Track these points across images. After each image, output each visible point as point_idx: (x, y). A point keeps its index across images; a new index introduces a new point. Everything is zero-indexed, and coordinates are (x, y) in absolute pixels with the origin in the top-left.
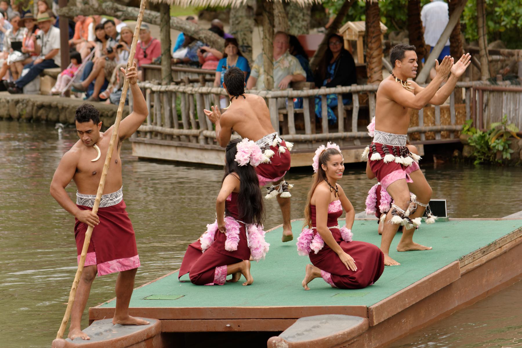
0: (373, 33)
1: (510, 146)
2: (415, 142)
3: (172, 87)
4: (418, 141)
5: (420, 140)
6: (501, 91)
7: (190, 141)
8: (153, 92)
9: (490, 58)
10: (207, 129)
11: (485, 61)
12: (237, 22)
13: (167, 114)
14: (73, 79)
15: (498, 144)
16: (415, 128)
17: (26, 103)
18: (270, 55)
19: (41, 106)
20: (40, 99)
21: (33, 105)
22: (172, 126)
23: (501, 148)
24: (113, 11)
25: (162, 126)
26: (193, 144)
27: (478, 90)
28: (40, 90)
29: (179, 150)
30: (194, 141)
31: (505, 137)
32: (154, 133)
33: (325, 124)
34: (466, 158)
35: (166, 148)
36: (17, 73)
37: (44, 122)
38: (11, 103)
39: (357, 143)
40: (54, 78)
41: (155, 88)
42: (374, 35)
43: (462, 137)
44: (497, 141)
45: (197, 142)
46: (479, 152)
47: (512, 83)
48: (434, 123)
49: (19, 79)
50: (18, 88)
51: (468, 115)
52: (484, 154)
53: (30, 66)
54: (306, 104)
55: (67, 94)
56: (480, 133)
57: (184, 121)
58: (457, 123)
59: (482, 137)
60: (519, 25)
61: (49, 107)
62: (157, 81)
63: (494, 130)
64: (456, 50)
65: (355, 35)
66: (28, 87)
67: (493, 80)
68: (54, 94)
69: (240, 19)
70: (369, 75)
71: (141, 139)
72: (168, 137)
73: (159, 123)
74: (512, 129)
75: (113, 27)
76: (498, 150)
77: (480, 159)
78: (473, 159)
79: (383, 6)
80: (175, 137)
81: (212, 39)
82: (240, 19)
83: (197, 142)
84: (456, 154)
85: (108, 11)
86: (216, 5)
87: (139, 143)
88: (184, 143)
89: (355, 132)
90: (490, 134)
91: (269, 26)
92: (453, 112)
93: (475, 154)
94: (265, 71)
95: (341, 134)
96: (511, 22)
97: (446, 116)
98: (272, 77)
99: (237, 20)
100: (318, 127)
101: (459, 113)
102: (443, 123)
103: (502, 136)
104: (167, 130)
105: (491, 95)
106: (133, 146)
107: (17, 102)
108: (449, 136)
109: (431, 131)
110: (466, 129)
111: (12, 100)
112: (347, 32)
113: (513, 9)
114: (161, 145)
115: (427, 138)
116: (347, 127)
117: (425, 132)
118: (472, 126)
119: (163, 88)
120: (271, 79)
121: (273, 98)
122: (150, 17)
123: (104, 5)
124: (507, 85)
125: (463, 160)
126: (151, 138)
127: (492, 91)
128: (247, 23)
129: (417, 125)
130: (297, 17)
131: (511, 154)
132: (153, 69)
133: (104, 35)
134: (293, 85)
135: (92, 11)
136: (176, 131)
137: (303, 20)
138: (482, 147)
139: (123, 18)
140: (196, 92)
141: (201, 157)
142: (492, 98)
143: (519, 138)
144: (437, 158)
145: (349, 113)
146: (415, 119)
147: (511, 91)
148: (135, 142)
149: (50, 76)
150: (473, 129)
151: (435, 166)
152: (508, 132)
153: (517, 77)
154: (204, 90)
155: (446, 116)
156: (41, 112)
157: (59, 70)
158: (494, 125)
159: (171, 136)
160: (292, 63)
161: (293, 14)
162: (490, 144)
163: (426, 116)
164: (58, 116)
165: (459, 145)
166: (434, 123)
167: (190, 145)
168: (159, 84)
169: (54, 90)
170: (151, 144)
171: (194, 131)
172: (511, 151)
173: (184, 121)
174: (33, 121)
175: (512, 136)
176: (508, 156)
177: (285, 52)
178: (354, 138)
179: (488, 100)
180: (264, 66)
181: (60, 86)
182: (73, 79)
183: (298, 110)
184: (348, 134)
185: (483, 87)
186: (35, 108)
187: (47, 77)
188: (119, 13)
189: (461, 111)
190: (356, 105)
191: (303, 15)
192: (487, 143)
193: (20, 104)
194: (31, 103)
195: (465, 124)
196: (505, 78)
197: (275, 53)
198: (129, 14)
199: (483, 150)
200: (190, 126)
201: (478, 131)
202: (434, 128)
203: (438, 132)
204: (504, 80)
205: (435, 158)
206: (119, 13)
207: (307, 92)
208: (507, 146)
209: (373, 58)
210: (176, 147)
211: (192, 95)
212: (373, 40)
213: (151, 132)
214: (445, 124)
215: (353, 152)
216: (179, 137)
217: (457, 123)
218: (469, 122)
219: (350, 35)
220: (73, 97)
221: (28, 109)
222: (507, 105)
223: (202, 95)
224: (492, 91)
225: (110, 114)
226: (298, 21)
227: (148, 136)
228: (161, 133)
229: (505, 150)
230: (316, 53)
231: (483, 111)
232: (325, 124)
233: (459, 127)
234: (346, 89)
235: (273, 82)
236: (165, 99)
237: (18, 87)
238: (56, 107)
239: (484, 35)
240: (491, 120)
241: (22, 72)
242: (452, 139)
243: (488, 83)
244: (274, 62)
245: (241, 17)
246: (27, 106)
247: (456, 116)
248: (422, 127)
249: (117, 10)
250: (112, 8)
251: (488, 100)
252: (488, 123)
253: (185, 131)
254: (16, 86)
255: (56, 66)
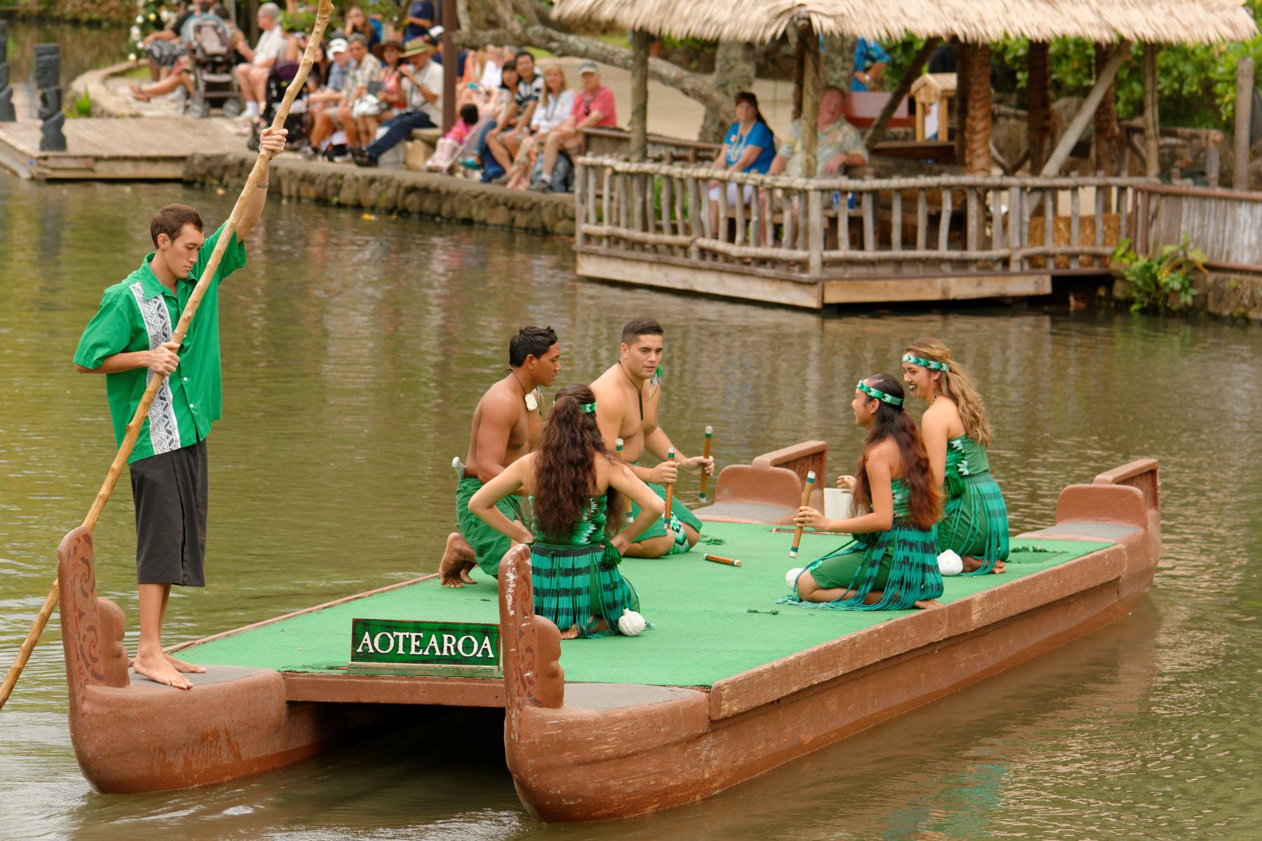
0: (978, 93)
1: (1192, 284)
2: (1037, 271)
3: (648, 167)
4: (1042, 270)
5: (1045, 267)
6: (1179, 196)
7: (673, 254)
8: (615, 173)
9: (1162, 142)
10: (703, 236)
11: (1153, 145)
12: (727, 67)
13: (637, 209)
14: (461, 148)
15: (1173, 279)
16: (1038, 249)
17: (387, 182)
18: (813, 121)
19: (412, 189)
20: (409, 178)
21: (399, 186)
22: (645, 228)
23: (1177, 286)
24: (544, 41)
25: (627, 227)
26: (680, 258)
27: (1142, 192)
28: (405, 163)
29: (655, 268)
30: (681, 254)
31: (1185, 269)
32: (615, 240)
33: (896, 235)
34: (1118, 301)
35: (635, 264)
36: (368, 133)
37: (415, 216)
38: (361, 181)
39: (946, 268)
40: (431, 145)
41: (621, 166)
42: (980, 96)
43: (1114, 266)
44: (1172, 275)
45: (686, 255)
46: (1139, 291)
47: (1196, 184)
48: (1069, 242)
49: (372, 142)
50: (370, 157)
51: (1124, 230)
52: (1148, 294)
53: (388, 123)
54: (867, 203)
55: (451, 171)
56: (1143, 261)
57: (665, 221)
58: (1104, 244)
59: (1147, 268)
60: (1185, 92)
61: (425, 191)
62: (623, 156)
63: (1167, 257)
64: (1105, 126)
65: (936, 95)
66: (386, 157)
67: (1165, 174)
68: (431, 170)
69: (733, 62)
70: (967, 160)
71: (593, 247)
72: (637, 247)
73: (623, 220)
74: (1197, 256)
75: (530, 65)
76: (1172, 290)
77: (1142, 302)
78: (1130, 301)
79: (265, 16)
80: (648, 246)
81: (703, 92)
82: (733, 62)
83: (686, 255)
84: (1102, 292)
85: (536, 41)
86: (732, 37)
87: (589, 254)
88: (666, 257)
89: (943, 251)
90: (1160, 263)
91: (814, 74)
92: (1100, 225)
93: (1135, 294)
94: (804, 147)
95: (921, 252)
96: (1171, 86)
97: (1088, 232)
98: (815, 157)
99: (728, 63)
100: (884, 240)
101: (1109, 227)
102: (1083, 243)
103: (1179, 267)
104: (637, 234)
105: (1163, 202)
106: (579, 258)
107: (372, 181)
108: (1091, 264)
109: (1063, 254)
110: (1120, 253)
111: (364, 177)
112: (922, 91)
113: (1175, 66)
114: (625, 259)
115: (1057, 266)
116: (932, 243)
117: (1053, 256)
118: (1129, 249)
119: (634, 167)
120: (813, 160)
121: (816, 190)
122: (605, 53)
123: (530, 31)
124: (1186, 185)
125: (1112, 304)
126: (609, 246)
127: (1164, 195)
128: (744, 70)
129: (1042, 243)
130: (832, 62)
131: (1194, 297)
132: (600, 137)
133: (514, 77)
134: (848, 169)
135: (509, 37)
136: (651, 237)
137: (843, 69)
138: (1146, 283)
139: (559, 52)
140: (688, 176)
141: (692, 281)
142: (1164, 205)
143: (1206, 272)
144: (1076, 299)
145: (934, 220)
146: (1038, 234)
147: (1196, 196)
148: (583, 253)
149: (423, 140)
150: (1132, 255)
151: (1072, 309)
152: (1189, 262)
153: (1203, 174)
154: (702, 172)
155: (1088, 232)
156: (412, 197)
157: (438, 131)
158: (1167, 250)
159: (642, 245)
160: (848, 138)
161: (827, 57)
162: (1159, 278)
163: (1057, 230)
164: (440, 206)
165: (1108, 280)
166: (1069, 242)
167: (674, 260)
168: (627, 160)
169: (430, 163)
170: (609, 257)
171: (681, 239)
172: (1194, 292)
173: (665, 221)
174: (398, 211)
175: (1196, 269)
176: (1189, 300)
177: (838, 119)
178: (941, 261)
179: (1157, 209)
180: (803, 139)
181: (441, 159)
182: (461, 148)
183: (854, 212)
184: (932, 254)
185: (1151, 187)
186: (402, 191)
187: (418, 143)
188: (554, 45)
189: (1112, 225)
190: (947, 208)
191: (844, 61)
192: (1154, 277)
193: (377, 184)
194: (394, 184)
195: (1119, 245)
196: (1185, 174)
197: (820, 121)
198: (569, 46)
199: (1148, 289)
200: (675, 230)
201: (1141, 257)
202: (1070, 249)
203: (1074, 256)
204: (1183, 177)
205: (1072, 299)
206: (554, 45)
207: (870, 183)
208: (1187, 284)
209: (977, 133)
210: (651, 263)
211: (681, 180)
212: (978, 105)
213: (608, 237)
214: (1086, 244)
215: (939, 282)
216: (655, 247)
217: (1104, 244)
218: (1125, 243)
219: (927, 95)
220: (459, 176)
221: (391, 193)
222: (1188, 218)
223: (697, 180)
224: (1164, 195)
225: (527, 205)
226: (834, 69)
227: (605, 243)
228: (625, 240)
229: (1184, 289)
230: (875, 123)
231: (1148, 225)
232: (896, 235)
233: (1108, 250)
234: (910, 182)
235: (816, 163)
236: (635, 185)
237: (370, 157)
238: (437, 191)
239: (1153, 105)
240: (1162, 240)
241: (375, 133)
242: (1095, 269)
243: (1158, 181)
244: (819, 134)
245: (735, 59)
246: (388, 187)
247: (1105, 233)
248: (1050, 247)
249: (551, 39)
250: (543, 36)
251: (1157, 209)
252: (1156, 245)
253: (667, 238)
254: (367, 154)
255: (433, 126)
